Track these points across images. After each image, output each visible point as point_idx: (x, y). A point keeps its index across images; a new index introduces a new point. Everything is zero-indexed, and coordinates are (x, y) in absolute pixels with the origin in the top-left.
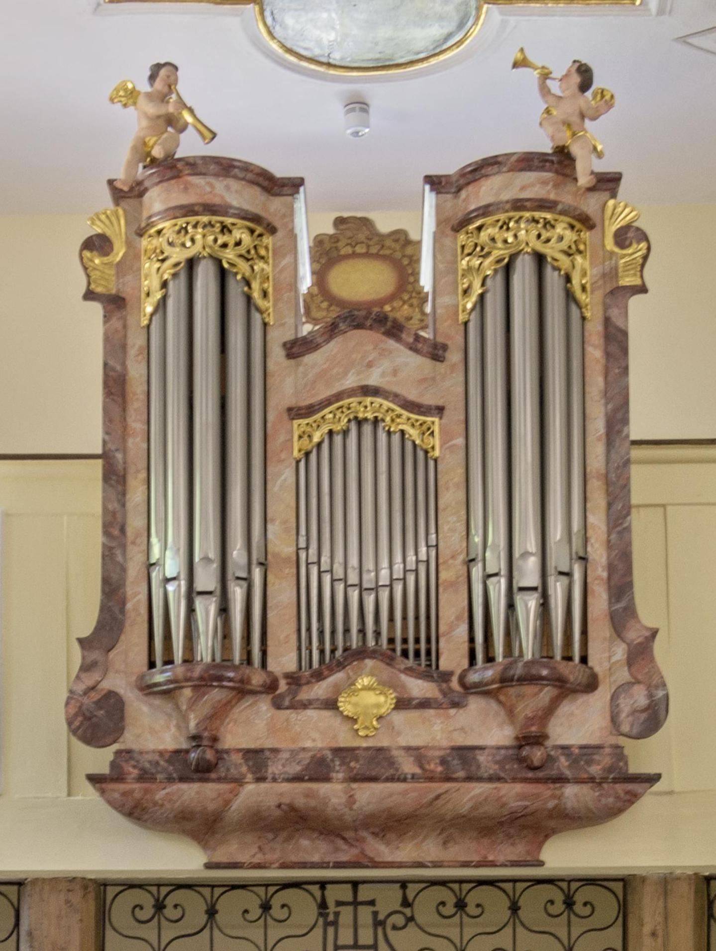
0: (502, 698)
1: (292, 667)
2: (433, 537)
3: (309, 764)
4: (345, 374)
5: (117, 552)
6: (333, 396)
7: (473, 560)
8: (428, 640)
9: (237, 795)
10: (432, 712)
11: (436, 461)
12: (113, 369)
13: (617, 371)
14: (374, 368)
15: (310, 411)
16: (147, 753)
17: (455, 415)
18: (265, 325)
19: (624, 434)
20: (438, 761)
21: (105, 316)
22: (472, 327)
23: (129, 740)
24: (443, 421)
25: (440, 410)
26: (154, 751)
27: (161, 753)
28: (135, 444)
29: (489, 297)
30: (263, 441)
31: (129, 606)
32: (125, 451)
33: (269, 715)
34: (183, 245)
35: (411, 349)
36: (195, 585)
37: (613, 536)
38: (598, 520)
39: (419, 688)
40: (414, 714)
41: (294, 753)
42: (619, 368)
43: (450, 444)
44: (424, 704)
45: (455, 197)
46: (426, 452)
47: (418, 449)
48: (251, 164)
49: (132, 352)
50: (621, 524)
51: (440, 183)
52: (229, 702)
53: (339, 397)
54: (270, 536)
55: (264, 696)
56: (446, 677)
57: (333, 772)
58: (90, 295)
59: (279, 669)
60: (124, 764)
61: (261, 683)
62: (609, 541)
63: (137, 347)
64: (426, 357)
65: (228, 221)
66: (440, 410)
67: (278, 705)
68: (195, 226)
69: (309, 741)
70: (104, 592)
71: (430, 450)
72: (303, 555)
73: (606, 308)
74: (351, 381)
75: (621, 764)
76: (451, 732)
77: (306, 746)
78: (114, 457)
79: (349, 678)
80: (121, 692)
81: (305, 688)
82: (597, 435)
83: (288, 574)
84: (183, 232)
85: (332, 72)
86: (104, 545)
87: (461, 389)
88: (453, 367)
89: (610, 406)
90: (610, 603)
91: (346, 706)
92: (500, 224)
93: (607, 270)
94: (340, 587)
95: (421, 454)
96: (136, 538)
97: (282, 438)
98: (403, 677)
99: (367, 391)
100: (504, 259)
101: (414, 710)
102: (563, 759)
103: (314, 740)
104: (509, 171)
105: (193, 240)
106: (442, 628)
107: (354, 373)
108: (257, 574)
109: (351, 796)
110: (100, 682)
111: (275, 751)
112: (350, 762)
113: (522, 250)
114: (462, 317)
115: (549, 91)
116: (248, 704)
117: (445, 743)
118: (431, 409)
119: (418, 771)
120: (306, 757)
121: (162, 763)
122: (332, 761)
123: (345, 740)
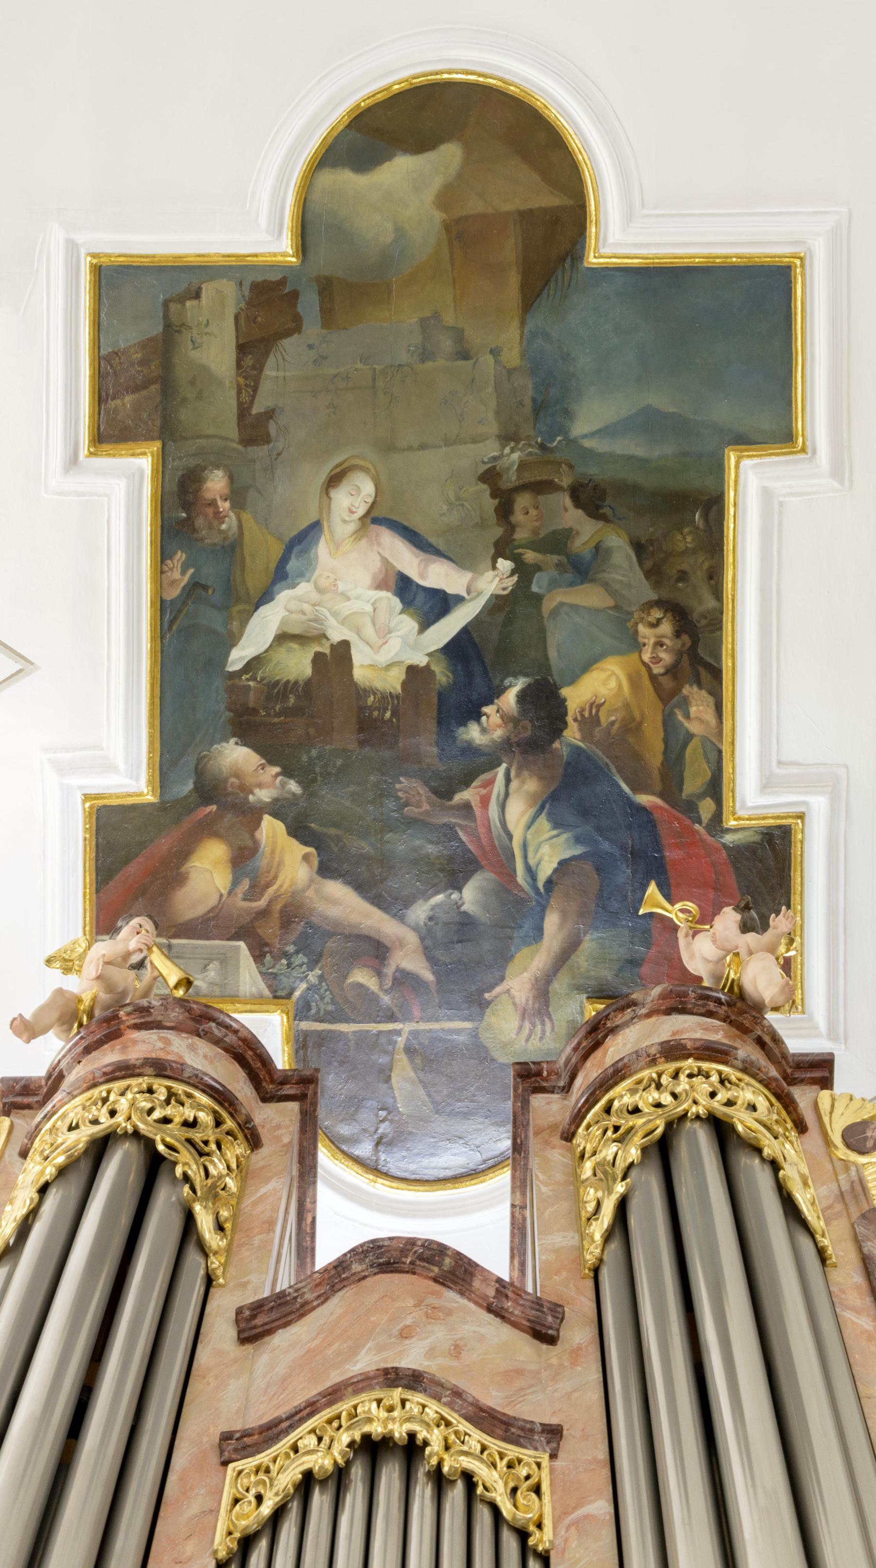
4: (354, 1352)
6: (323, 1395)
18: (209, 1281)
22: (605, 1275)
24: (557, 1463)
25: (554, 1433)
35: (490, 1309)
43: (580, 1513)
45: (565, 1099)
46: (523, 1535)
51: (539, 1074)
53: (334, 1395)
71: (532, 1528)
87: (597, 1395)
88: (576, 1353)
97: (194, 1508)
104: (648, 1015)
107: (370, 1349)
114: (590, 1258)
118: (532, 1431)
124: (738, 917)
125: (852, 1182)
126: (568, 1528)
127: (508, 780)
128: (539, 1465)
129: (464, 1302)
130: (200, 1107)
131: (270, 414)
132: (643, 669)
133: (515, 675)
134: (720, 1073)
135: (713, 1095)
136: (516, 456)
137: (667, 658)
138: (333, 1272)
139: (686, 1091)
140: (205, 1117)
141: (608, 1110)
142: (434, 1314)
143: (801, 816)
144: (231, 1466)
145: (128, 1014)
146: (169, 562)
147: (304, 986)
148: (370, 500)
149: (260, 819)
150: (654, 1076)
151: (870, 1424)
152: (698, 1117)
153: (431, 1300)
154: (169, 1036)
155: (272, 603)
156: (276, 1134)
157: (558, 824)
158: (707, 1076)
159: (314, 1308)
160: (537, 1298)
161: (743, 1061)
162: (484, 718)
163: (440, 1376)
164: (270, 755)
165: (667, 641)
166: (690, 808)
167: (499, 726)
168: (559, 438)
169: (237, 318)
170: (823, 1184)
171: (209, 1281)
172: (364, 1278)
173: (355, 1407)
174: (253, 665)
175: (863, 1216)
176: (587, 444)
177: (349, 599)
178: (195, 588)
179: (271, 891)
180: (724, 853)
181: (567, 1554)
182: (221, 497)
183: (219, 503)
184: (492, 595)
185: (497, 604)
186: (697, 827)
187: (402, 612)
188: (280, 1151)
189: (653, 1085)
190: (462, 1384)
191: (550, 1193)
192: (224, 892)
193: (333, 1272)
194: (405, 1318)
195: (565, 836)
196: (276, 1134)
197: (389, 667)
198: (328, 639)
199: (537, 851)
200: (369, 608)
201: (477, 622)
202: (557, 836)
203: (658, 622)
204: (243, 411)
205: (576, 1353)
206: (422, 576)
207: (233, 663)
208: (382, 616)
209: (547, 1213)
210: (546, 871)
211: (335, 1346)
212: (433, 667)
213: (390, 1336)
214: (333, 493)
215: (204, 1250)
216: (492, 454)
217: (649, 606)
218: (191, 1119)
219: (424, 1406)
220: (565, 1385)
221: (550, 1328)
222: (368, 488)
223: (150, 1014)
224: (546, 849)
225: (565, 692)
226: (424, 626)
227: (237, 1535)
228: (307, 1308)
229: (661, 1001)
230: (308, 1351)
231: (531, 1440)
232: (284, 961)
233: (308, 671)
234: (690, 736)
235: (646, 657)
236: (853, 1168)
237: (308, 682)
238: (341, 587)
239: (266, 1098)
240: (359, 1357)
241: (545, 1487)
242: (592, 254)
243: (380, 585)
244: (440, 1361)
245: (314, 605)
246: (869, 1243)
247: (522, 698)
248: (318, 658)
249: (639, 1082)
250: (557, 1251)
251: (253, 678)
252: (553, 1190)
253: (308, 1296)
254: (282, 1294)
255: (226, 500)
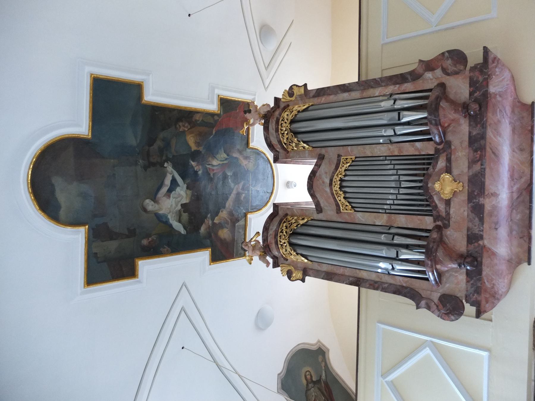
0: (446, 125)
1: (431, 218)
2: (381, 158)
3: (474, 214)
4: (326, 191)
5: (384, 286)
7: (390, 141)
8: (424, 159)
9: (490, 249)
10: (453, 157)
11: (356, 158)
12: (324, 276)
13: (328, 91)
14: (324, 181)
15: (337, 205)
16: (467, 288)
17: (341, 151)
18: (312, 220)
19: (348, 85)
20: (475, 153)
21: (309, 276)
22: (314, 145)
23: (461, 294)
24: (343, 155)
25: (339, 156)
26: (466, 285)
27: (468, 282)
28: (347, 272)
29: (305, 140)
30: (347, 224)
31: (404, 285)
32: (350, 276)
33: (452, 230)
34: (286, 246)
35: (319, 167)
36: (394, 257)
37: (383, 84)
38: (377, 91)
39: (441, 163)
40: (454, 165)
41: (471, 221)
42: (328, 90)
43: (350, 152)
44: (449, 160)
45: (280, 153)
46: (353, 161)
47: (352, 164)
48: (266, 221)
49: (319, 268)
50: (379, 82)
52: (444, 248)
53: (333, 194)
54: (380, 224)
55: (443, 232)
56: (437, 151)
57: (479, 202)
58: (303, 280)
59: (432, 224)
60: (472, 300)
61: (436, 233)
62: (385, 86)
63: (317, 266)
64: (322, 162)
65: (280, 230)
66: (339, 156)
67: (447, 226)
68: (281, 242)
69: (465, 213)
70: (398, 295)
72: (387, 211)
73: (310, 98)
74: (328, 189)
75: (479, 67)
76: (462, 148)
77: (467, 214)
78: (351, 281)
79: (436, 194)
80: (439, 294)
81: (441, 214)
82: (348, 96)
83: (394, 218)
84: (282, 246)
85: (274, 192)
86: (381, 291)
88: (326, 152)
89: (339, 92)
90: (408, 82)
91: (446, 197)
92: (282, 136)
93: (300, 99)
94: (399, 197)
95: (354, 163)
96: (379, 277)
98: (436, 170)
99: (331, 184)
100: (292, 134)
101: (452, 165)
102: (476, 95)
103: (464, 211)
104: (269, 134)
105: (284, 243)
106: (417, 153)
108: (393, 231)
109: (492, 195)
110: (434, 303)
111: (468, 229)
112: (474, 195)
113: (289, 128)
114: (311, 148)
115: (252, 123)
116: (447, 240)
117: (467, 151)
119: (479, 163)
120: (472, 215)
121: (472, 282)
122: (474, 203)
123: (464, 197)
124: (247, 113)
127: (209, 165)
128: (343, 159)
130: (283, 226)
131: (128, 229)
132: (189, 130)
133: (189, 162)
134: (281, 121)
135: (286, 123)
136: (141, 161)
137: (187, 125)
139: (285, 128)
140: (285, 225)
141: (285, 144)
143: (219, 96)
144: (341, 211)
145: (265, 244)
146: (163, 252)
147: (243, 210)
148: (150, 200)
149: (215, 223)
150: (281, 134)
152: (290, 126)
155: (172, 225)
157: (217, 153)
158: (282, 124)
160: (318, 158)
161: (279, 116)
162: (197, 170)
164: (202, 222)
165: (184, 124)
166: (216, 121)
167: (199, 166)
168: (137, 149)
169: (102, 241)
171: (312, 220)
173: (335, 190)
174: (185, 228)
175: (306, 96)
176: (138, 141)
177: (172, 205)
178: (169, 245)
179: (227, 219)
180: (225, 115)
182: (148, 240)
183: (150, 240)
184: (172, 168)
185: (174, 167)
186: (219, 120)
187: (175, 191)
189: (283, 135)
190: (331, 172)
192: (227, 230)
195: (220, 152)
197: (186, 194)
198: (180, 209)
199: (222, 158)
200: (174, 199)
201: (177, 172)
202: (220, 153)
203: (179, 126)
204: (128, 237)
206: (168, 186)
207: (184, 233)
208: (175, 196)
210: (225, 156)
212: (187, 183)
214: (148, 210)
216: (140, 168)
217: (176, 128)
218: (285, 227)
219: (335, 178)
222: (148, 201)
223: (265, 239)
224: (222, 156)
225: (193, 150)
226: (178, 185)
227: (351, 209)
232: (239, 215)
233: (187, 214)
234: (202, 120)
235: (186, 129)
236: (297, 97)
237: (189, 214)
238: (169, 207)
239: (278, 213)
241: (346, 157)
242: (89, 137)
243: (169, 197)
245: (173, 213)
246: (311, 96)
247: (193, 161)
248: (184, 212)
249: (282, 137)
250: (309, 155)
251: (188, 227)
253: (316, 200)
255: (149, 239)
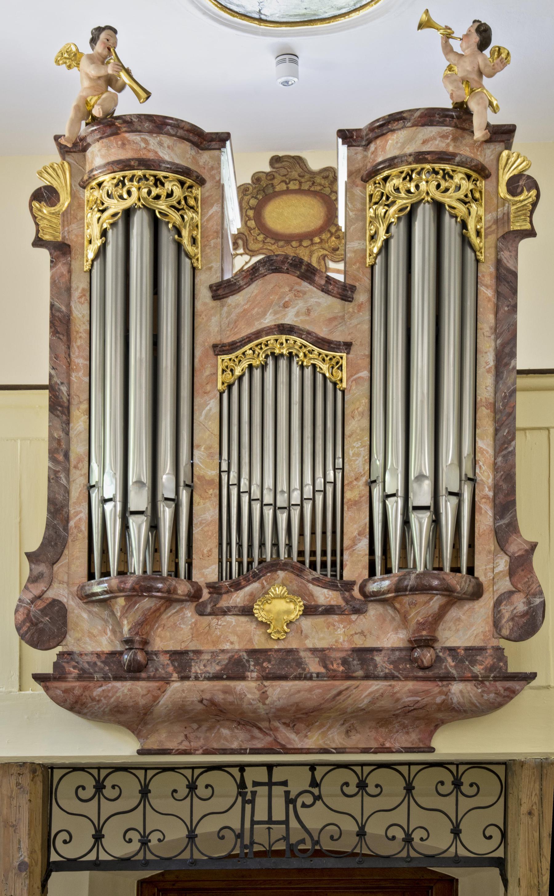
4: (264, 314)
24: (350, 356)
25: (348, 346)
35: (323, 291)
46: (335, 384)
53: (258, 334)
71: (338, 382)
87: (367, 327)
107: (271, 313)
125: (504, 214)
126: (352, 382)
129: (311, 287)
138: (251, 271)
142: (299, 294)
151: (478, 341)
153: (297, 287)
154: (147, 137)
156: (212, 173)
159: (244, 289)
163: (301, 326)
170: (490, 212)
172: (266, 275)
181: (351, 392)
188: (216, 186)
191: (354, 216)
193: (251, 271)
194: (285, 297)
196: (212, 173)
205: (360, 306)
209: (352, 229)
211: (256, 309)
213: (279, 307)
215: (188, 255)
220: (354, 322)
221: (350, 297)
228: (241, 288)
229: (419, 119)
230: (244, 310)
231: (339, 349)
240: (266, 317)
244: (301, 318)
246: (502, 253)
252: (356, 214)
254: (229, 281)
